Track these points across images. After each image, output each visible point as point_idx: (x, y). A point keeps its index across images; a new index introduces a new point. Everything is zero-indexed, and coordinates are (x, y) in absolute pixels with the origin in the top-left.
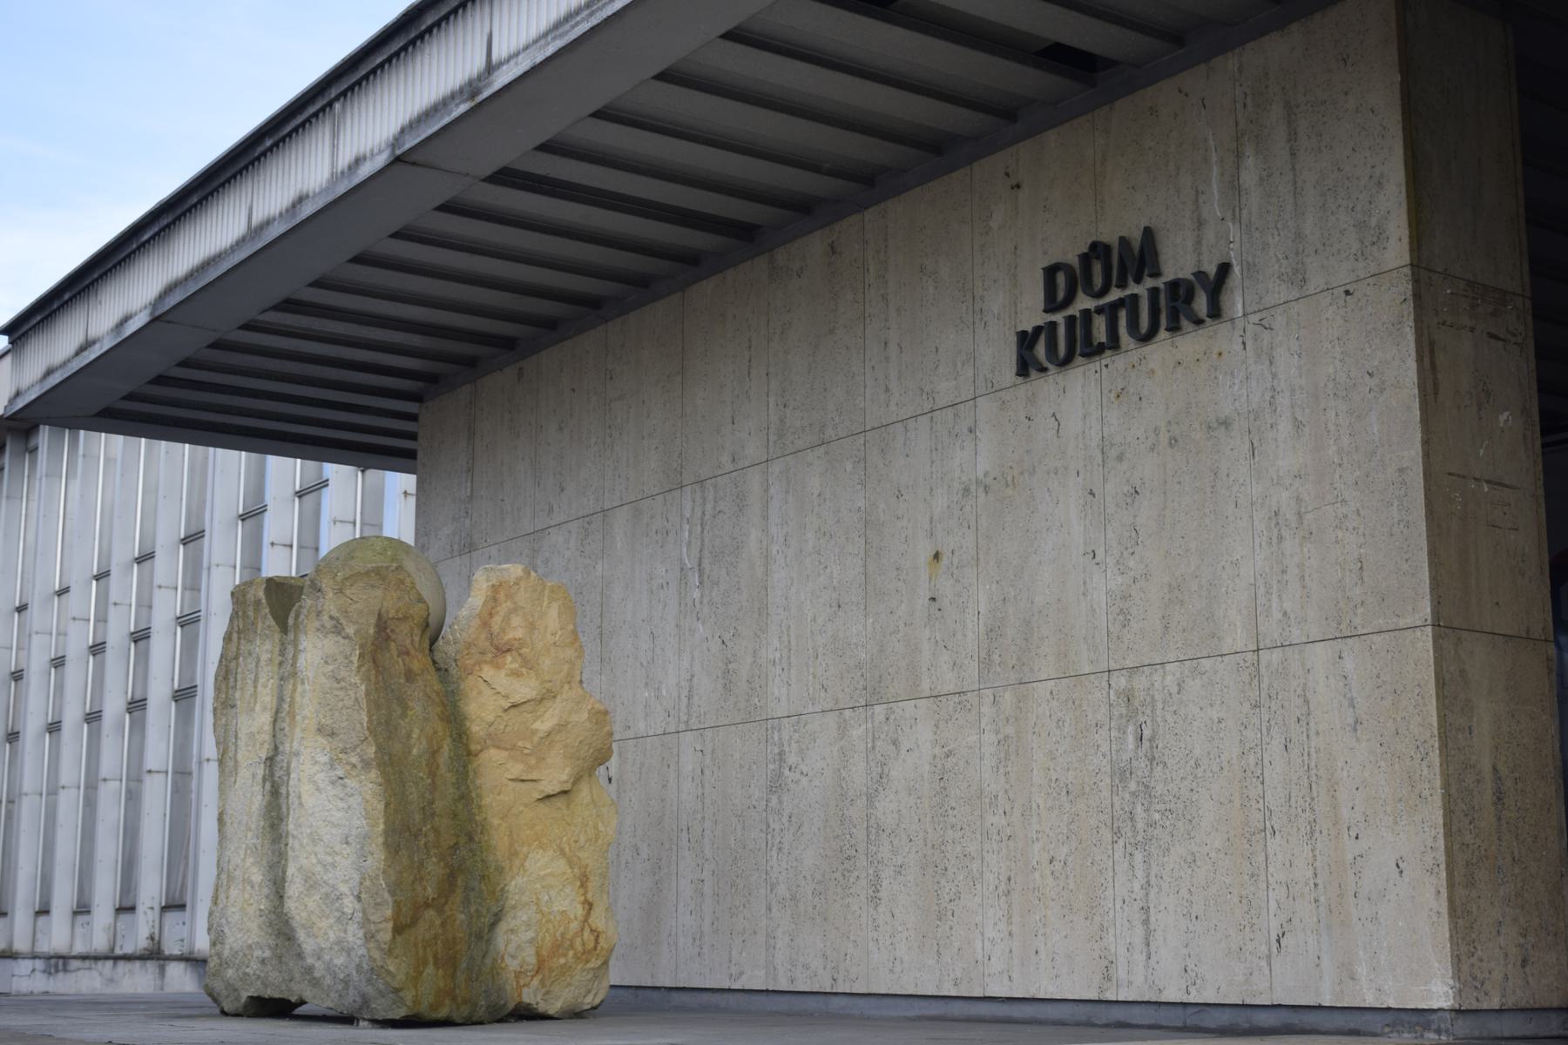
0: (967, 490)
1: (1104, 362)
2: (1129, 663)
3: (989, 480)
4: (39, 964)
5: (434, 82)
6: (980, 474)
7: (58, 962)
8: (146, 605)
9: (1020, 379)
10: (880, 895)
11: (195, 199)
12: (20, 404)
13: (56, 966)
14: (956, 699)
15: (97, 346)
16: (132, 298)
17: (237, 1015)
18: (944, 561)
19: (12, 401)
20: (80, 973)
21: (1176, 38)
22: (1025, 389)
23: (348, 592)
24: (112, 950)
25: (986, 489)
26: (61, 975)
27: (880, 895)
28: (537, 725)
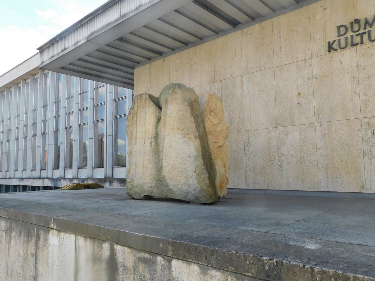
0: (309, 79)
1: (357, 47)
2: (368, 116)
3: (317, 76)
4: (17, 180)
5: (107, 20)
6: (314, 75)
7: (22, 179)
8: (27, 121)
9: (328, 53)
10: (283, 168)
11: (100, 12)
12: (44, 64)
13: (21, 180)
14: (307, 125)
15: (68, 49)
16: (82, 36)
17: (140, 199)
18: (302, 95)
19: (41, 64)
20: (26, 181)
21: (201, 39)
22: (329, 55)
23: (184, 94)
24: (6, 177)
25: (316, 78)
26: (22, 182)
27: (283, 168)
28: (217, 130)
